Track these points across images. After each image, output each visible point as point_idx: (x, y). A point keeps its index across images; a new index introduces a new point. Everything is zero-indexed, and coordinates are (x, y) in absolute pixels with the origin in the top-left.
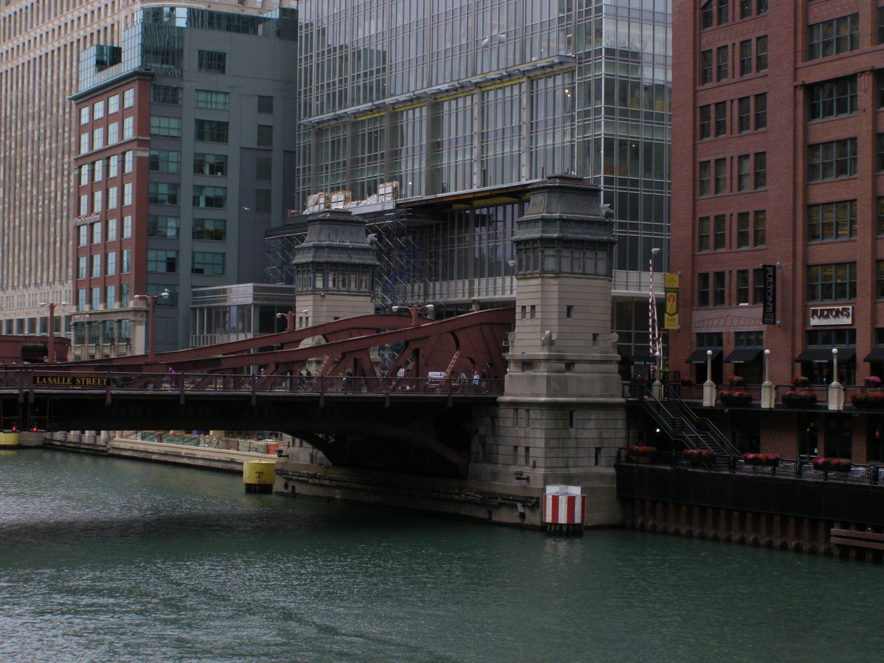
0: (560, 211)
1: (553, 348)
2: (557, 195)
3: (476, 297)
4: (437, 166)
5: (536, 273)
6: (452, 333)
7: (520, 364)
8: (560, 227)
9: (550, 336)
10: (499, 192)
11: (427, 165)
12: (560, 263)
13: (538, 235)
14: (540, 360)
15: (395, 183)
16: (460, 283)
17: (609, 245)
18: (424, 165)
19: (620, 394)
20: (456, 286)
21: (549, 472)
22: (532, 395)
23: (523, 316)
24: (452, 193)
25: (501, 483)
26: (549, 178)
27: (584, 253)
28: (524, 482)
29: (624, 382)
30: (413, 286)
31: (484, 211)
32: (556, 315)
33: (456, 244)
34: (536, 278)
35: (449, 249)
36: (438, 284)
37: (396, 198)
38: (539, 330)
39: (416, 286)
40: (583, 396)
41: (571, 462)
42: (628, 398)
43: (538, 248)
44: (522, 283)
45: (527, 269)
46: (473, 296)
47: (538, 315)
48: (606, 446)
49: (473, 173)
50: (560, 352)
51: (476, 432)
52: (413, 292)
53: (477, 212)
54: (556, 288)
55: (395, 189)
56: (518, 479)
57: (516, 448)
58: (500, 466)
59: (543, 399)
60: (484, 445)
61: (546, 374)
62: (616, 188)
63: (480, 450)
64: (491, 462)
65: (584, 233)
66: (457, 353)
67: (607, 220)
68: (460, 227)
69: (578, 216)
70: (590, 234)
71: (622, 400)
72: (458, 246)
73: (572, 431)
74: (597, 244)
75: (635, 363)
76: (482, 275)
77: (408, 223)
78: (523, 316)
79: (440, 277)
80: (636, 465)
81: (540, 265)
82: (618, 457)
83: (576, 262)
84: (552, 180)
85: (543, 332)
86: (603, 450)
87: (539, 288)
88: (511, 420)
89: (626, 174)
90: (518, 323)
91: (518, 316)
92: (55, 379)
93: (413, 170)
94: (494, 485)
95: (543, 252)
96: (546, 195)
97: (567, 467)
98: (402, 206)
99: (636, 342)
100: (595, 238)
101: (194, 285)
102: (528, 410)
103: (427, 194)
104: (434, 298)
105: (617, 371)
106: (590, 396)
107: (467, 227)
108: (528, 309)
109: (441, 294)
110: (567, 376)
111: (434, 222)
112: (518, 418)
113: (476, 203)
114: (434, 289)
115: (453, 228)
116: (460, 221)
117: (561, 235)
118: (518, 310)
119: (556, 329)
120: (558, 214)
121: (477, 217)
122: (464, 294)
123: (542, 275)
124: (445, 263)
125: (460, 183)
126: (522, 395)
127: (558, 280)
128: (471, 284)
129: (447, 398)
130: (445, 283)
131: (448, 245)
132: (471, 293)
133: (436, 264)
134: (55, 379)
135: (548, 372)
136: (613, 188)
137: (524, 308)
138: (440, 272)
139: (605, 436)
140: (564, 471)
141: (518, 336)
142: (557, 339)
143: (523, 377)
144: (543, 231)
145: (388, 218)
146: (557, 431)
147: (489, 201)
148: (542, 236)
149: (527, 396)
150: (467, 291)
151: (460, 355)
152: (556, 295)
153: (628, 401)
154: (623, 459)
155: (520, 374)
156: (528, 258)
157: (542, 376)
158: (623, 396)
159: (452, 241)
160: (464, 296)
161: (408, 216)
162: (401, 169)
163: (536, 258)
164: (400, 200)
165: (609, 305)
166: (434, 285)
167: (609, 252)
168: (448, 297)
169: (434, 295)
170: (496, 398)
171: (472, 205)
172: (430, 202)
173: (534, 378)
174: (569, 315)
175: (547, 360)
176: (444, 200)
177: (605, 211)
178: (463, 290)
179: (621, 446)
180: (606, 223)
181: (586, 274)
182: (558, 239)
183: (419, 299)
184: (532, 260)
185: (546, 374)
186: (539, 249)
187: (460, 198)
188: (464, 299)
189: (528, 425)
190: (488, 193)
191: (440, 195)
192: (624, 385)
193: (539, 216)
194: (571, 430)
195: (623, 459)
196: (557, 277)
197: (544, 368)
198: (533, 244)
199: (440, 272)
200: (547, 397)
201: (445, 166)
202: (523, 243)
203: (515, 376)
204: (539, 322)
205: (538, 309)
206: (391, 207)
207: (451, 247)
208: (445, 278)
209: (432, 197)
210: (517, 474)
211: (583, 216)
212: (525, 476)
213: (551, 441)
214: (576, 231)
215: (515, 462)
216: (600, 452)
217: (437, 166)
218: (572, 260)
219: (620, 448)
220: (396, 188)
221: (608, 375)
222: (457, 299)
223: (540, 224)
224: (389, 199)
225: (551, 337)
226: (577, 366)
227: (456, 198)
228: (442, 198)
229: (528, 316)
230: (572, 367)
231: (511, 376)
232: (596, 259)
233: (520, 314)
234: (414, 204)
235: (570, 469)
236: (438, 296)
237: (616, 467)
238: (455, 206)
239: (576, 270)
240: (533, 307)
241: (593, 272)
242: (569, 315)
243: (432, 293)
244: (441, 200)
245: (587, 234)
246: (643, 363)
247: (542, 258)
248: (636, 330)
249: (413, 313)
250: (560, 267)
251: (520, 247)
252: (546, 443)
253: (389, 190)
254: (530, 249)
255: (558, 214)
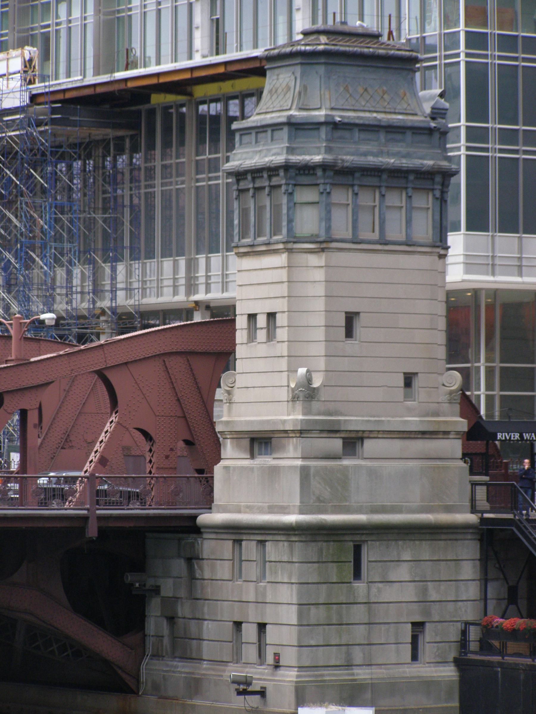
0: (328, 106)
1: (315, 405)
2: (322, 69)
3: (200, 296)
4: (119, 11)
5: (277, 243)
6: (101, 374)
7: (246, 443)
8: (327, 140)
9: (309, 380)
10: (244, 66)
11: (97, 11)
12: (328, 219)
13: (280, 159)
14: (286, 432)
15: (29, 51)
16: (168, 264)
17: (438, 179)
18: (90, 10)
19: (468, 504)
20: (160, 271)
21: (307, 676)
22: (272, 510)
23: (252, 337)
24: (153, 69)
25: (208, 703)
26: (306, 34)
27: (383, 196)
28: (254, 701)
29: (477, 478)
30: (69, 273)
31: (215, 108)
32: (320, 334)
33: (158, 181)
34: (276, 252)
35: (143, 191)
36: (121, 268)
37: (30, 82)
38: (285, 368)
39: (77, 272)
40: (383, 510)
41: (358, 656)
42: (483, 512)
43: (280, 186)
44: (248, 263)
45: (259, 233)
46: (196, 292)
47: (282, 334)
48: (437, 618)
49: (194, 26)
50: (330, 414)
51: (156, 590)
52: (69, 287)
53: (203, 108)
54: (320, 275)
55: (28, 64)
56: (240, 693)
57: (238, 625)
58: (205, 665)
59: (292, 518)
60: (172, 619)
61: (299, 463)
62: (493, 57)
63: (166, 631)
64: (186, 657)
65: (380, 153)
66: (113, 418)
67: (433, 124)
68: (167, 144)
69: (367, 115)
70: (394, 155)
71: (472, 518)
72: (163, 185)
73: (360, 586)
74: (411, 177)
75: (499, 436)
76: (214, 249)
77: (54, 135)
78: (252, 337)
79: (127, 253)
80: (497, 658)
81: (285, 223)
82: (463, 643)
83: (365, 218)
84: (312, 37)
85: (292, 370)
86: (428, 625)
87: (283, 275)
88: (227, 565)
89: (512, 24)
90: (241, 351)
91: (241, 336)
92: (508, 438)
93: (70, 21)
94: (193, 706)
95: (291, 194)
96: (298, 69)
97: (349, 665)
98: (41, 99)
99: (502, 389)
100: (405, 163)
101: (486, 266)
102: (262, 543)
103: (97, 72)
104: (114, 298)
105: (459, 454)
106: (394, 510)
107: (182, 142)
108: (262, 321)
109: (129, 290)
110: (346, 467)
111: (111, 133)
112: (241, 561)
113: (200, 91)
114: (113, 278)
115: (151, 146)
116: (167, 130)
117: (329, 157)
118: (241, 322)
119: (321, 364)
120: (323, 112)
121: (201, 119)
122: (175, 287)
123: (290, 246)
124: (135, 221)
125: (166, 49)
126: (250, 509)
127: (324, 255)
128: (191, 266)
129: (85, 519)
130: (136, 265)
131: (143, 184)
132: (191, 287)
133: (117, 223)
134: (508, 438)
135: (304, 458)
136: (486, 56)
137: (252, 317)
138: (127, 242)
139: (434, 596)
140: (342, 675)
141: (241, 380)
142: (324, 385)
143: (251, 469)
144: (290, 150)
145: (10, 125)
146: (324, 586)
147: (227, 87)
148: (287, 161)
149: (261, 511)
150: (182, 281)
151: (118, 423)
152: (320, 290)
153: (483, 520)
154: (473, 646)
155: (247, 463)
156: (260, 210)
157: (290, 467)
158: (473, 510)
159: (150, 173)
160: (175, 293)
161: (53, 122)
162: (57, 17)
163: (276, 209)
164: (38, 87)
165: (441, 309)
166: (114, 270)
167: (438, 194)
168: (144, 295)
169: (114, 291)
170: (194, 518)
171: (191, 94)
172: (99, 90)
173: (274, 471)
174: (349, 333)
175: (301, 432)
176: (130, 85)
177: (432, 103)
178: (175, 279)
179: (470, 617)
180: (430, 131)
181: (386, 243)
182: (324, 167)
183: (82, 301)
184: (267, 215)
185: (299, 463)
186: (283, 188)
187: (162, 80)
188: (177, 298)
189: (263, 575)
190: (221, 70)
191: (120, 75)
192: (474, 484)
193: (280, 117)
194: (357, 585)
195: (473, 646)
196: (323, 250)
197: (295, 449)
198: (270, 177)
199: (127, 242)
200: (301, 512)
201: (136, 13)
202: (249, 177)
203: (235, 468)
204: (283, 349)
205: (281, 320)
206: (17, 103)
207: (146, 187)
208: (135, 256)
209: (104, 78)
210: (239, 683)
211: (380, 116)
212: (256, 686)
213: (313, 610)
214: (364, 148)
215: (237, 657)
216: (423, 632)
217: (119, 11)
218: (355, 214)
219: (467, 624)
220: (31, 60)
221: (439, 463)
222: (161, 300)
223: (285, 133)
224: (16, 83)
225: (309, 380)
226: (368, 444)
227: (154, 81)
228: (126, 80)
229: (262, 335)
230: (358, 445)
231: (226, 468)
232: (410, 210)
233: (245, 332)
234: (68, 95)
235: (356, 670)
236: (121, 294)
237: (459, 663)
238: (157, 99)
239: (365, 234)
240: (271, 316)
241: (402, 237)
242: (349, 333)
243: (108, 288)
244: (122, 86)
245: (389, 154)
246: (517, 436)
247: (289, 209)
248: (502, 361)
249: (12, 332)
250: (328, 229)
251: (243, 185)
252: (300, 615)
253: (16, 64)
254: (263, 188)
255: (323, 112)
